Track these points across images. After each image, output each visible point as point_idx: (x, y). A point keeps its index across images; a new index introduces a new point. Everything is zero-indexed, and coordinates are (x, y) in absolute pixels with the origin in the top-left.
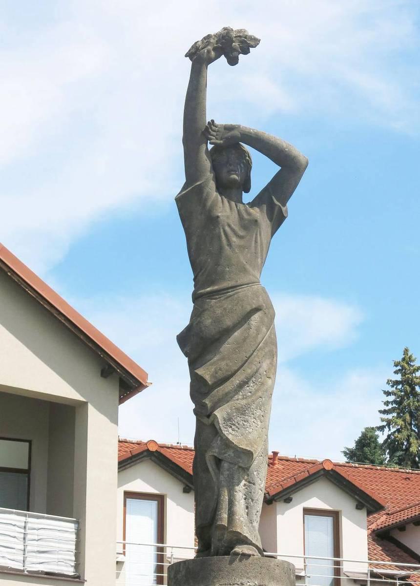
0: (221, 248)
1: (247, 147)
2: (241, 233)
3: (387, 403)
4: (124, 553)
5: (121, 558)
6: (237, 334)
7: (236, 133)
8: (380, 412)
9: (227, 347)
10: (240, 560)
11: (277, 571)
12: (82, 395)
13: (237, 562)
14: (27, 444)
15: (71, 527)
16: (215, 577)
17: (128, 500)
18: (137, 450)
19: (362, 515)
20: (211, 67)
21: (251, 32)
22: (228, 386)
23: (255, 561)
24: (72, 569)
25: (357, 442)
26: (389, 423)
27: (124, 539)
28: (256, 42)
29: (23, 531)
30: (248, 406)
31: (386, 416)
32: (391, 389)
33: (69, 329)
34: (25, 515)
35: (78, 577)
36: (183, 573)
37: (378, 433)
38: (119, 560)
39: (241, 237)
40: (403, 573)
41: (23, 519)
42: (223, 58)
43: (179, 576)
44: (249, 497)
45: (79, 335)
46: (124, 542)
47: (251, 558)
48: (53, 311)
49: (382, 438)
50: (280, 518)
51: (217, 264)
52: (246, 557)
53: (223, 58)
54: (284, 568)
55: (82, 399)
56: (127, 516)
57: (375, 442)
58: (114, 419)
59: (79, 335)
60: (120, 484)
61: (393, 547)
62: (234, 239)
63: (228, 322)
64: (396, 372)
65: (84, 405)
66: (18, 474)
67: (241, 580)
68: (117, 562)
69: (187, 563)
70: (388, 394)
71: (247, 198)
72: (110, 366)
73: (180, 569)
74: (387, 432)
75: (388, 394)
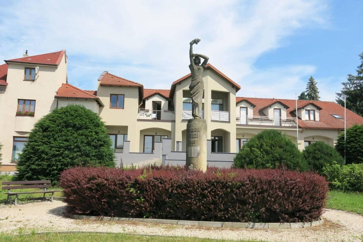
0: (194, 73)
1: (199, 57)
2: (198, 70)
3: (307, 87)
6: (196, 86)
7: (197, 55)
8: (306, 89)
9: (195, 88)
15: (228, 113)
17: (241, 108)
18: (242, 99)
19: (285, 109)
20: (193, 45)
21: (199, 39)
22: (195, 94)
25: (301, 95)
26: (308, 91)
28: (200, 40)
30: (198, 97)
31: (307, 89)
32: (308, 84)
37: (305, 93)
39: (197, 71)
40: (293, 119)
42: (195, 44)
44: (198, 110)
49: (306, 94)
50: (269, 110)
51: (194, 75)
53: (195, 44)
57: (304, 94)
58: (235, 95)
61: (293, 114)
62: (196, 72)
63: (195, 84)
64: (309, 81)
70: (308, 85)
71: (200, 65)
74: (307, 92)
75: (308, 85)
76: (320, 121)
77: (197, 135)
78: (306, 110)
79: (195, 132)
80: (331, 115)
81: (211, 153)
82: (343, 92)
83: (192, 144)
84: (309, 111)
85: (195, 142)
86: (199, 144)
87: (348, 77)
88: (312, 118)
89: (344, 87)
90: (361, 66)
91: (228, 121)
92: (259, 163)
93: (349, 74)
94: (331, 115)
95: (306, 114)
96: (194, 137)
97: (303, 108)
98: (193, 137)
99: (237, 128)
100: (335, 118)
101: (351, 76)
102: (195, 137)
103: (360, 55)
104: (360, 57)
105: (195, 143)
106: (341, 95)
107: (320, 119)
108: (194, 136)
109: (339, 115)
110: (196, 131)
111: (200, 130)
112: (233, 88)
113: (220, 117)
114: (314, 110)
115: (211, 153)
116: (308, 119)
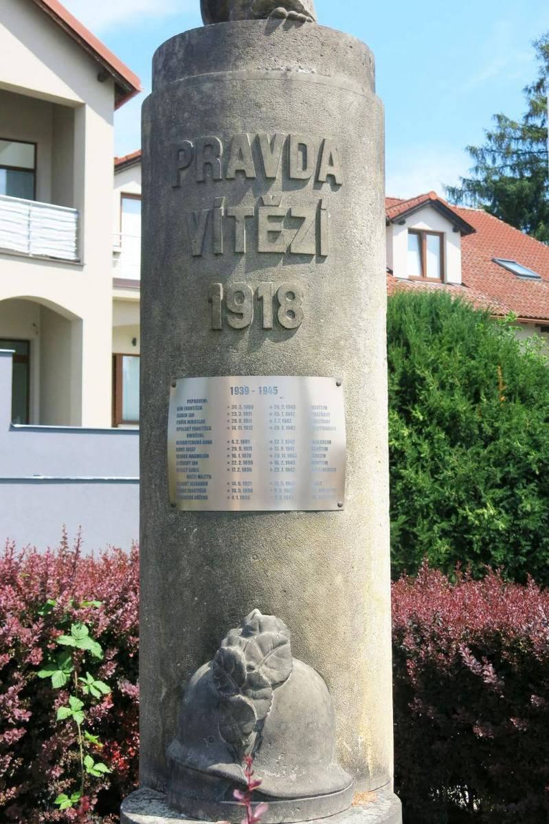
4: (121, 246)
5: (117, 250)
10: (286, 28)
11: (350, 56)
12: (80, 97)
13: (279, 31)
14: (32, 147)
15: (73, 217)
16: (239, 58)
17: (124, 200)
23: (313, 31)
24: (74, 254)
27: (121, 231)
29: (27, 218)
33: (69, 36)
34: (29, 204)
35: (79, 261)
36: (180, 55)
38: (116, 251)
41: (27, 207)
43: (173, 62)
45: (76, 38)
46: (120, 234)
47: (305, 25)
48: (52, 15)
52: (296, 22)
54: (361, 54)
55: (81, 101)
56: (123, 213)
59: (76, 38)
60: (116, 185)
65: (82, 106)
66: (27, 173)
67: (286, 64)
68: (115, 253)
69: (187, 35)
72: (105, 70)
73: (174, 50)
76: (463, 284)
77: (309, 224)
78: (411, 231)
79: (293, 183)
80: (493, 261)
81: (12, 429)
82: (468, 185)
83: (255, 345)
84: (420, 235)
85: (286, 321)
86: (336, 345)
87: (494, 128)
88: (433, 271)
89: (473, 162)
90: (540, 86)
91: (72, 257)
92: (420, 502)
93: (499, 113)
94: (493, 261)
95: (410, 249)
96: (279, 247)
97: (402, 223)
98: (264, 246)
99: (116, 301)
100: (512, 276)
101: (507, 120)
102: (291, 256)
103: (535, 44)
104: (535, 52)
105: (288, 332)
106: (461, 196)
107: (463, 277)
108: (274, 235)
109: (526, 264)
110: (296, 172)
111: (345, 166)
112: (97, 82)
113: (32, 234)
114: (441, 235)
115: (12, 429)
116: (416, 272)
